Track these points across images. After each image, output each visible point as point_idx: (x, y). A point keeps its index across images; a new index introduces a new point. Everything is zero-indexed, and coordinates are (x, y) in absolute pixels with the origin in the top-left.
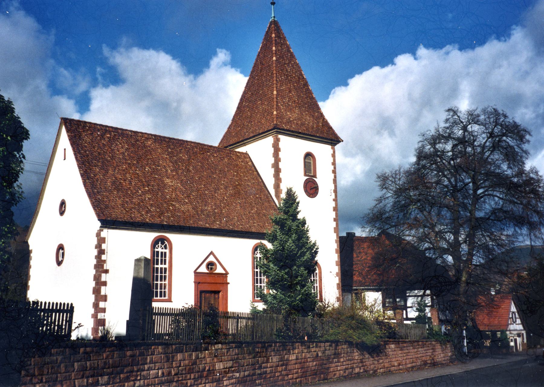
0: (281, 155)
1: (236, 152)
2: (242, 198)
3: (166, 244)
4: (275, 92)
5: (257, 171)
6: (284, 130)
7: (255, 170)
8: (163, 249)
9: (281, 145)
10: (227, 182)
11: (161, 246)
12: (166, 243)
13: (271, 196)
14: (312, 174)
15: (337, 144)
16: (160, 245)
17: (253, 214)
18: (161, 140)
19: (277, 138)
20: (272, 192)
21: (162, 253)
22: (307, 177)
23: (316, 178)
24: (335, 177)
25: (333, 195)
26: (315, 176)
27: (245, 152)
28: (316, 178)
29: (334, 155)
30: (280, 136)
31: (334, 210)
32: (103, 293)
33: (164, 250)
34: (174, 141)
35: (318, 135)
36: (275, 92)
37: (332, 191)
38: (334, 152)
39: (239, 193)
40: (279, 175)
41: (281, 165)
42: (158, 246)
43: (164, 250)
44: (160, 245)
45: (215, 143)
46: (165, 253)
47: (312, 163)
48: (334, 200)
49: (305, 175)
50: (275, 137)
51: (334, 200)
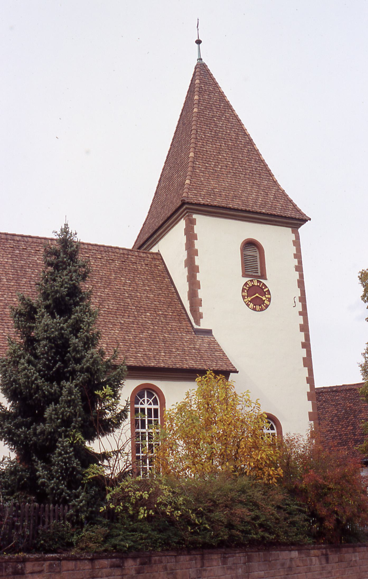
0: (197, 244)
1: (153, 253)
2: (129, 316)
3: (155, 397)
4: (192, 154)
5: (170, 278)
6: (199, 205)
7: (37, 239)
8: (150, 404)
9: (197, 229)
10: (108, 294)
11: (148, 401)
12: (156, 395)
13: (186, 313)
14: (259, 274)
15: (303, 224)
16: (146, 398)
17: (141, 338)
18: (7, 239)
19: (189, 219)
20: (187, 305)
21: (149, 410)
22: (247, 279)
23: (266, 279)
24: (301, 276)
25: (299, 305)
26: (263, 276)
27: (157, 251)
28: (266, 279)
29: (297, 243)
30: (194, 216)
31: (301, 330)
32: (296, 260)
33: (153, 407)
34: (29, 239)
35: (264, 211)
36: (192, 154)
37: (297, 300)
38: (298, 237)
39: (126, 309)
40: (195, 277)
41: (198, 261)
42: (144, 401)
43: (153, 407)
44: (146, 398)
45: (130, 246)
46: (156, 410)
47: (258, 257)
48: (300, 313)
49: (245, 275)
50: (187, 218)
51: (300, 313)
